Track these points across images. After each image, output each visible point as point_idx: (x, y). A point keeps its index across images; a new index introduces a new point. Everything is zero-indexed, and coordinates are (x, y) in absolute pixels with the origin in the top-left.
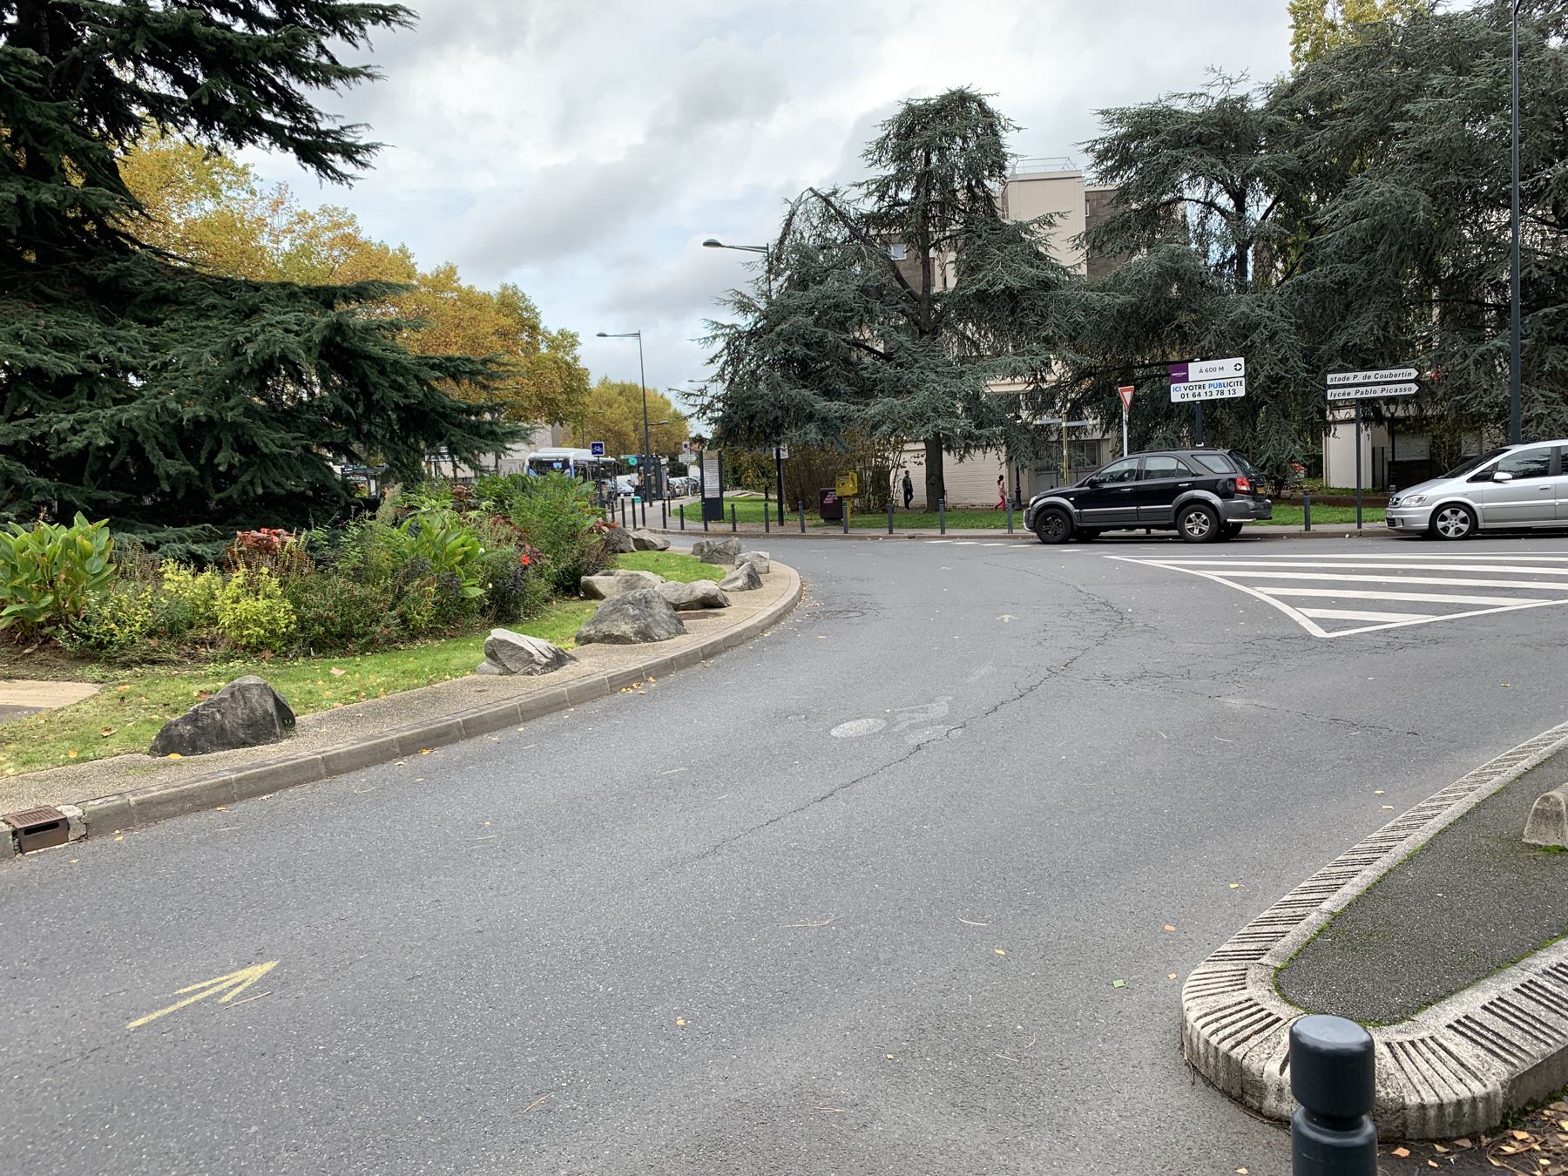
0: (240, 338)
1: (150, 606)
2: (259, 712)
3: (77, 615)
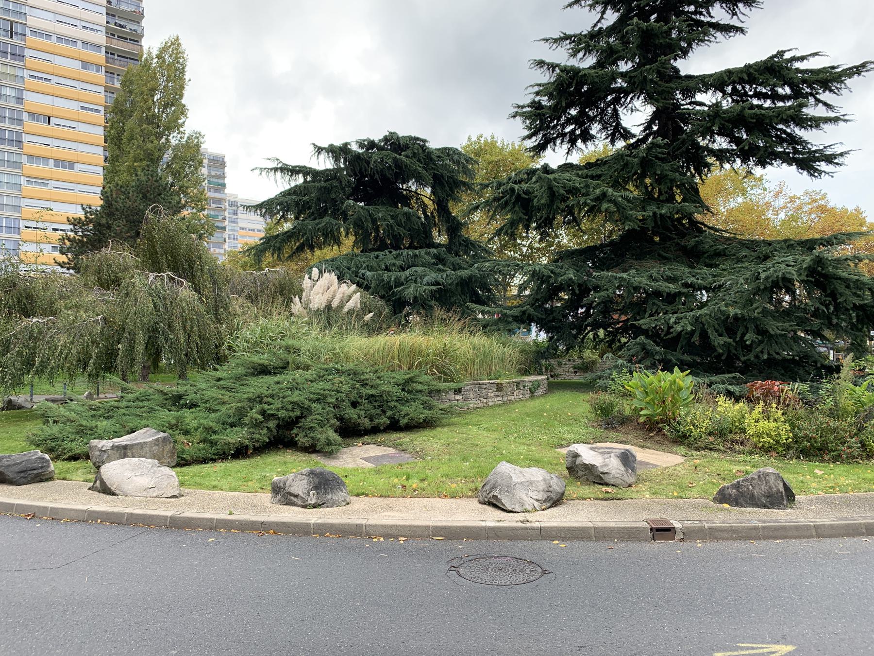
0: (760, 270)
1: (710, 419)
2: (774, 489)
3: (675, 419)
